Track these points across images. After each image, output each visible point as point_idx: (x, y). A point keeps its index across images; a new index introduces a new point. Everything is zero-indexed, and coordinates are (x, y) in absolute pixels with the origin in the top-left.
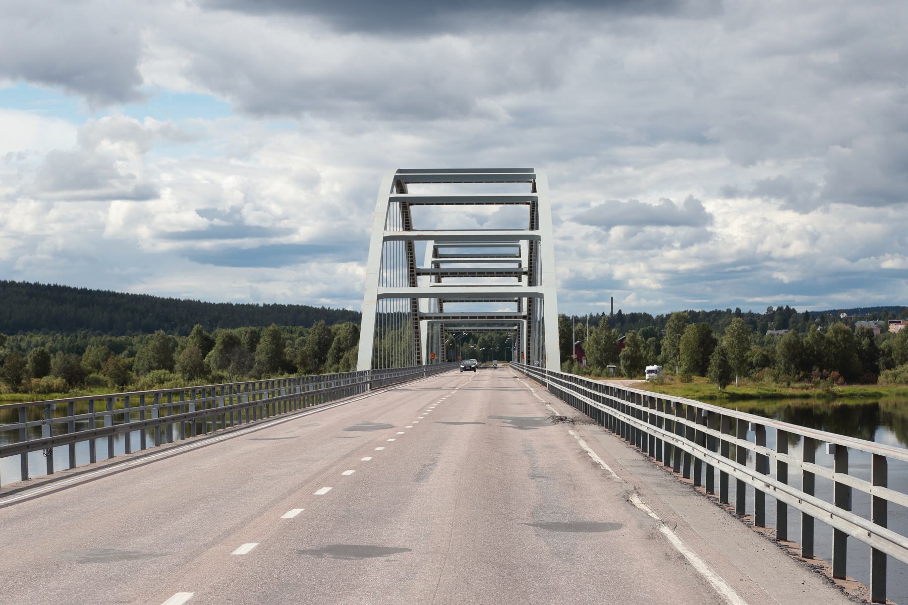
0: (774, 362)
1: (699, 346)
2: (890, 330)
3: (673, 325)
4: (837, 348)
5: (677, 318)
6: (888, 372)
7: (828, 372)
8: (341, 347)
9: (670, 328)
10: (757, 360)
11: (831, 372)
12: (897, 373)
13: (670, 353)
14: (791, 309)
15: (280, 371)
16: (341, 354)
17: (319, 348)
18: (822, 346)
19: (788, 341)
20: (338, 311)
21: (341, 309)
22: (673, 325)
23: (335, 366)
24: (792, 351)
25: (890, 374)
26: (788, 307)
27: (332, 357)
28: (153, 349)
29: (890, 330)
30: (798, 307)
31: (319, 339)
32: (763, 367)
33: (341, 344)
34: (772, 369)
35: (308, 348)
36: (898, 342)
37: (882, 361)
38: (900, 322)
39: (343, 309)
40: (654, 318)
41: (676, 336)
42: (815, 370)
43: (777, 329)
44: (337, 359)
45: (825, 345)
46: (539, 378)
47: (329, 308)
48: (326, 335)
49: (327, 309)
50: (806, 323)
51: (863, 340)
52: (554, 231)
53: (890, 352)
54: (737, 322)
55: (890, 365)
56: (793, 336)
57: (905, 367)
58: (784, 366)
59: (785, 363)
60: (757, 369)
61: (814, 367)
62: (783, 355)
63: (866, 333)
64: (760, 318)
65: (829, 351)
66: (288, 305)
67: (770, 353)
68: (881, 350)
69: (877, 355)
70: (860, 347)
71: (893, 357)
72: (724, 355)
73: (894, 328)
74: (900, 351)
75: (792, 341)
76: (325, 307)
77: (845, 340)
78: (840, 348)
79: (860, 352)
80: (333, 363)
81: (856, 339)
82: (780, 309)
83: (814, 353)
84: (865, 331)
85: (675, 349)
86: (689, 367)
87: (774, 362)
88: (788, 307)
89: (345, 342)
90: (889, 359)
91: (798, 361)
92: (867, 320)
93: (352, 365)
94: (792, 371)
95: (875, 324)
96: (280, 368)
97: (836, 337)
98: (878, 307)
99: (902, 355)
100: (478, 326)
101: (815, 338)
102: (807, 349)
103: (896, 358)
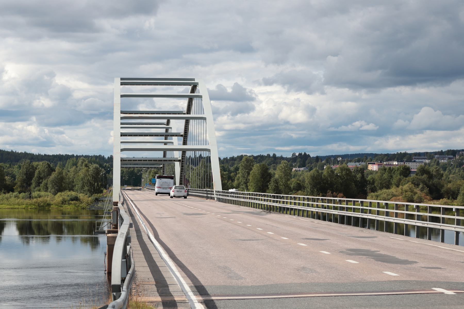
0: (304, 188)
1: (261, 178)
2: (368, 168)
3: (243, 165)
4: (342, 179)
5: (246, 160)
6: (372, 194)
7: (337, 194)
8: (41, 176)
9: (242, 167)
10: (294, 186)
11: (338, 194)
12: (378, 195)
13: (242, 181)
14: (307, 154)
15: (3, 191)
16: (41, 181)
17: (26, 177)
18: (333, 178)
19: (313, 175)
20: (21, 153)
21: (23, 152)
22: (243, 165)
23: (37, 188)
24: (315, 181)
25: (374, 195)
26: (305, 154)
27: (35, 182)
28: (309, 181)
29: (368, 168)
30: (312, 153)
31: (27, 171)
32: (298, 190)
33: (41, 175)
34: (303, 192)
35: (20, 176)
36: (378, 176)
37: (369, 187)
38: (375, 163)
39: (25, 152)
40: (222, 160)
41: (245, 171)
42: (329, 193)
43: (299, 167)
44: (38, 184)
45: (335, 177)
46: (206, 195)
47: (16, 151)
48: (31, 169)
49: (15, 152)
50: (317, 163)
51: (358, 175)
52: (215, 120)
53: (373, 182)
54: (284, 163)
55: (374, 190)
56: (316, 172)
57: (383, 191)
58: (310, 190)
59: (311, 188)
60: (294, 191)
61: (329, 191)
62: (310, 183)
63: (360, 170)
64: (288, 160)
65: (337, 181)
66: (65, 155)
67: (301, 182)
68: (368, 181)
69: (366, 184)
70: (356, 179)
71: (375, 185)
72: (277, 183)
73: (373, 167)
74: (380, 181)
75: (315, 175)
76: (13, 151)
77: (347, 174)
78: (344, 180)
79: (356, 182)
80: (36, 187)
81: (353, 174)
82: (300, 154)
83: (328, 182)
84: (359, 169)
85: (244, 179)
86: (255, 190)
87: (304, 188)
88: (305, 154)
89: (43, 173)
90: (373, 186)
91: (319, 187)
92: (354, 162)
93: (49, 187)
94: (315, 193)
95: (360, 164)
96: (3, 189)
97: (342, 173)
98: (359, 154)
99: (381, 184)
100: (141, 165)
101: (329, 173)
102: (324, 180)
103: (377, 186)
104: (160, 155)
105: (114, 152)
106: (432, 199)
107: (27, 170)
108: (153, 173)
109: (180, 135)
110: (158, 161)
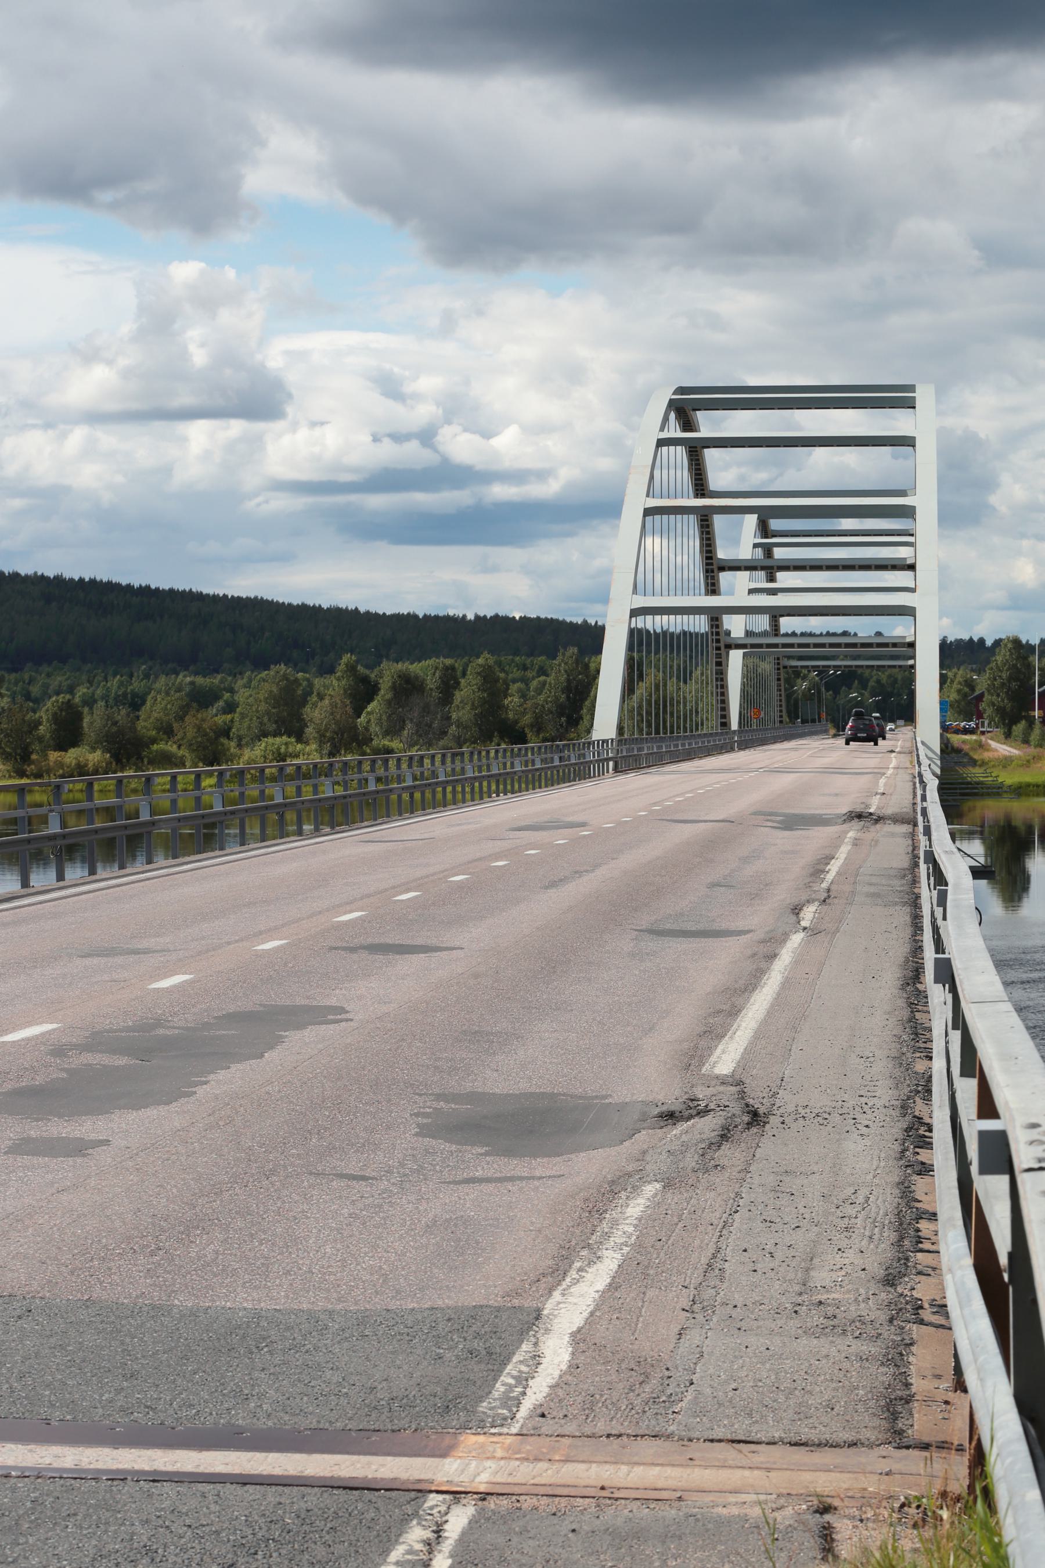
17: (568, 697)
31: (568, 681)
47: (596, 622)
48: (580, 673)
49: (593, 624)
76: (589, 621)
96: (496, 734)
104: (699, 624)
105: (608, 619)
106: (272, 727)
107: (568, 676)
108: (960, 683)
109: (905, 565)
110: (783, 647)
